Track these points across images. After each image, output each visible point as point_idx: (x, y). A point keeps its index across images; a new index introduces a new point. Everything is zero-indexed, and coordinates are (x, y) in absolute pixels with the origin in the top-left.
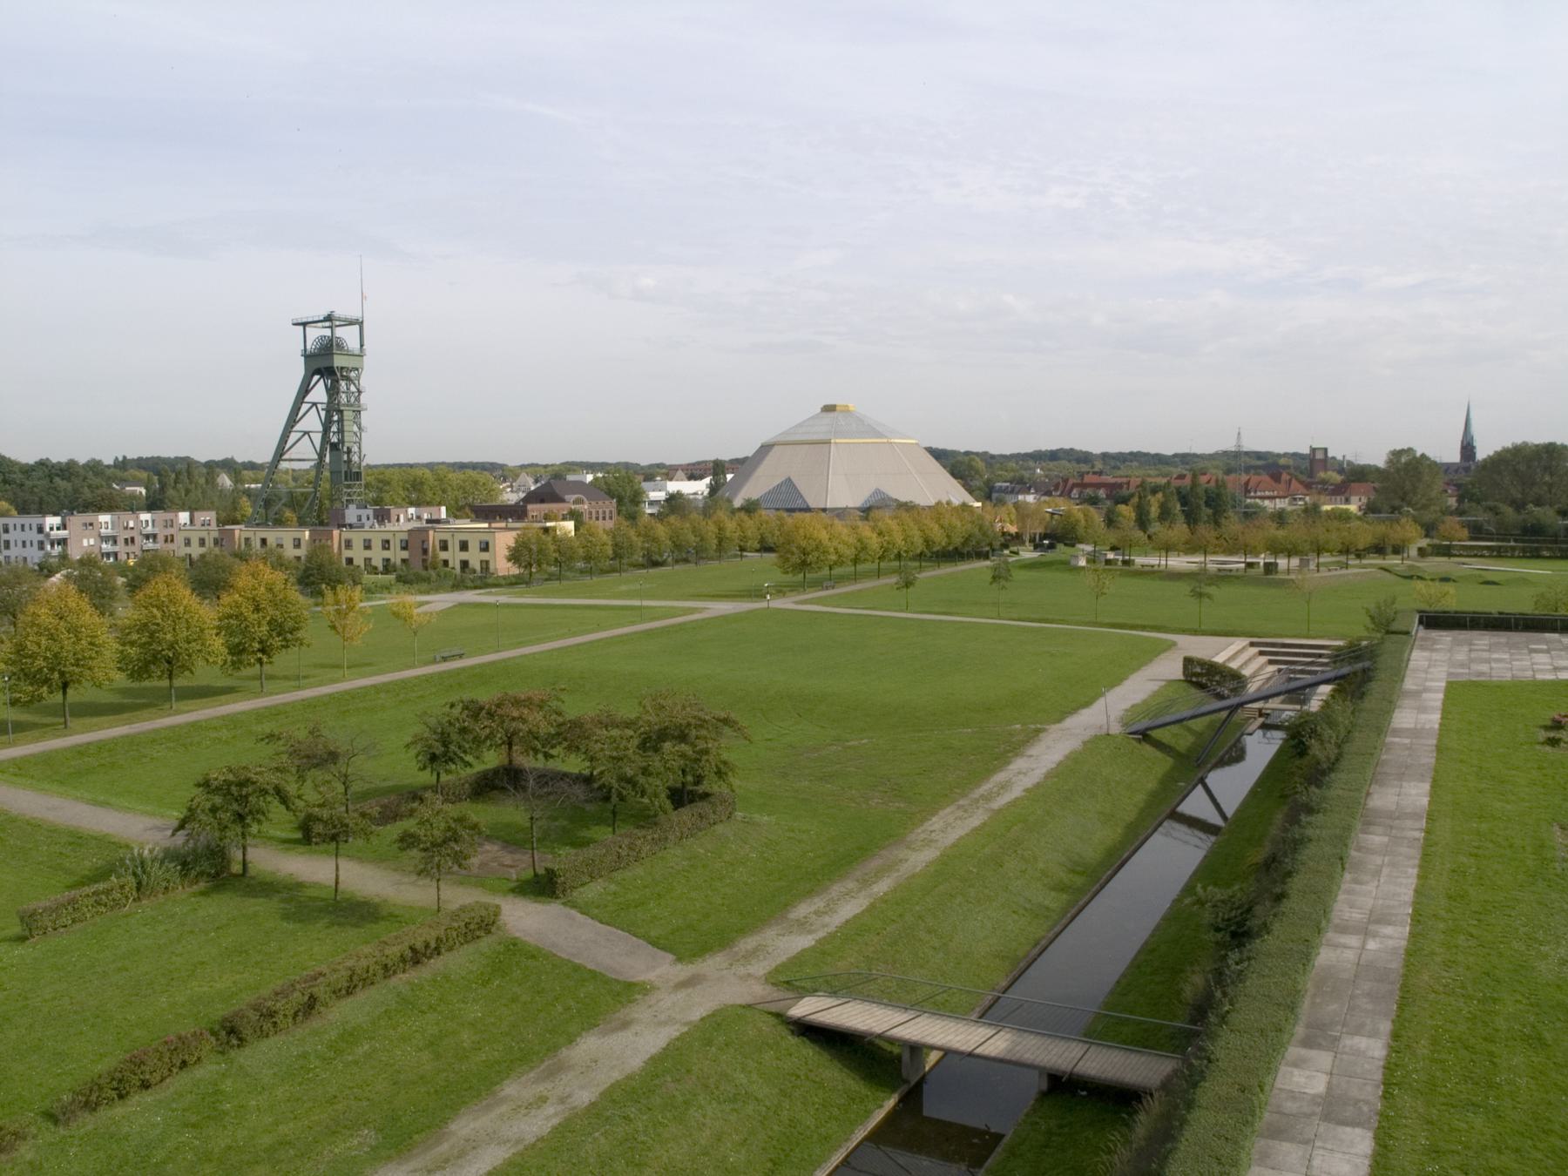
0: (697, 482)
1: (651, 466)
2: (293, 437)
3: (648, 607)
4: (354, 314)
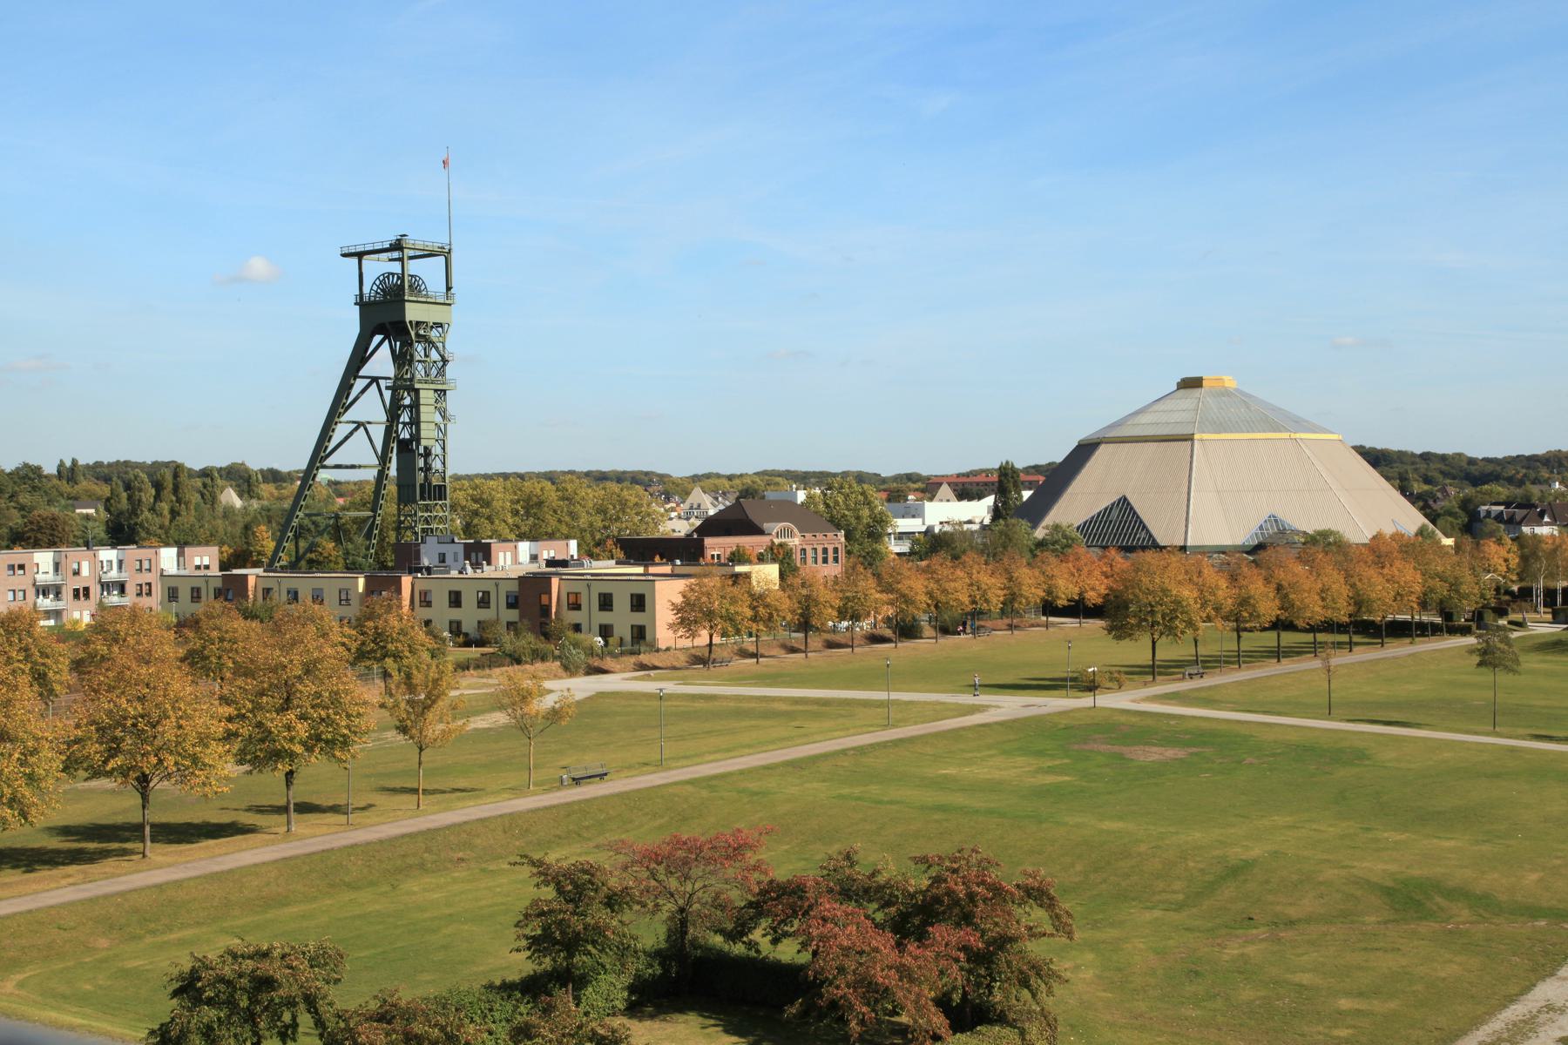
0: (974, 503)
2: (340, 431)
3: (897, 702)
4: (437, 239)
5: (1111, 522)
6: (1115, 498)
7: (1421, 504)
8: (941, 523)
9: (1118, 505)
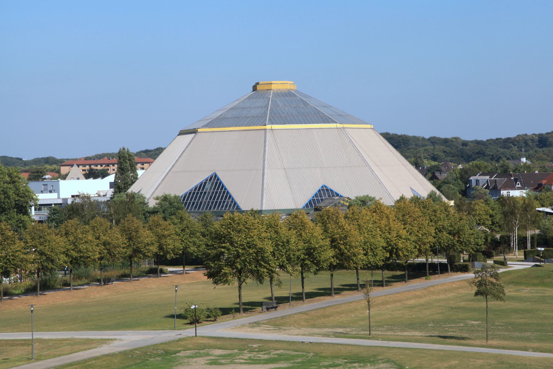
0: (99, 180)
1: (37, 161)
3: (40, 341)
5: (205, 193)
6: (208, 175)
7: (430, 175)
8: (73, 196)
9: (210, 180)
